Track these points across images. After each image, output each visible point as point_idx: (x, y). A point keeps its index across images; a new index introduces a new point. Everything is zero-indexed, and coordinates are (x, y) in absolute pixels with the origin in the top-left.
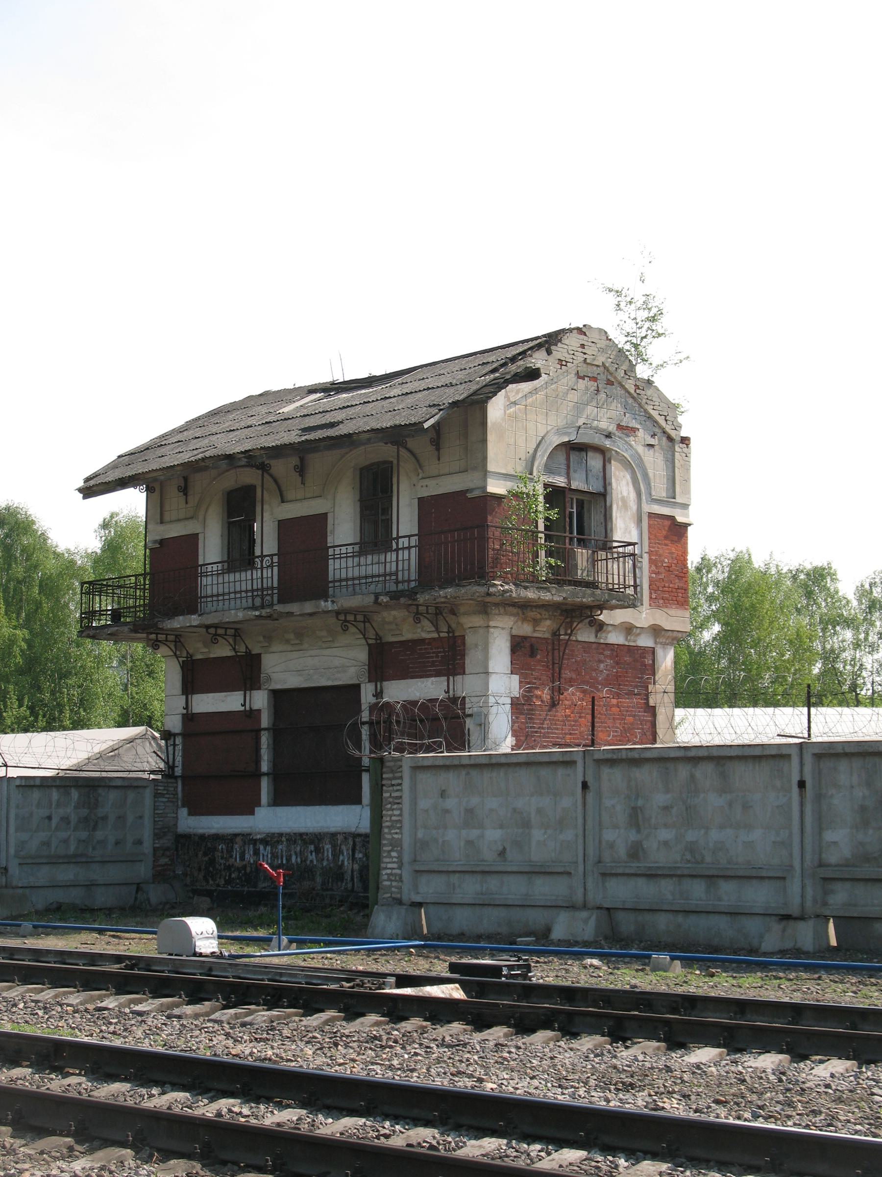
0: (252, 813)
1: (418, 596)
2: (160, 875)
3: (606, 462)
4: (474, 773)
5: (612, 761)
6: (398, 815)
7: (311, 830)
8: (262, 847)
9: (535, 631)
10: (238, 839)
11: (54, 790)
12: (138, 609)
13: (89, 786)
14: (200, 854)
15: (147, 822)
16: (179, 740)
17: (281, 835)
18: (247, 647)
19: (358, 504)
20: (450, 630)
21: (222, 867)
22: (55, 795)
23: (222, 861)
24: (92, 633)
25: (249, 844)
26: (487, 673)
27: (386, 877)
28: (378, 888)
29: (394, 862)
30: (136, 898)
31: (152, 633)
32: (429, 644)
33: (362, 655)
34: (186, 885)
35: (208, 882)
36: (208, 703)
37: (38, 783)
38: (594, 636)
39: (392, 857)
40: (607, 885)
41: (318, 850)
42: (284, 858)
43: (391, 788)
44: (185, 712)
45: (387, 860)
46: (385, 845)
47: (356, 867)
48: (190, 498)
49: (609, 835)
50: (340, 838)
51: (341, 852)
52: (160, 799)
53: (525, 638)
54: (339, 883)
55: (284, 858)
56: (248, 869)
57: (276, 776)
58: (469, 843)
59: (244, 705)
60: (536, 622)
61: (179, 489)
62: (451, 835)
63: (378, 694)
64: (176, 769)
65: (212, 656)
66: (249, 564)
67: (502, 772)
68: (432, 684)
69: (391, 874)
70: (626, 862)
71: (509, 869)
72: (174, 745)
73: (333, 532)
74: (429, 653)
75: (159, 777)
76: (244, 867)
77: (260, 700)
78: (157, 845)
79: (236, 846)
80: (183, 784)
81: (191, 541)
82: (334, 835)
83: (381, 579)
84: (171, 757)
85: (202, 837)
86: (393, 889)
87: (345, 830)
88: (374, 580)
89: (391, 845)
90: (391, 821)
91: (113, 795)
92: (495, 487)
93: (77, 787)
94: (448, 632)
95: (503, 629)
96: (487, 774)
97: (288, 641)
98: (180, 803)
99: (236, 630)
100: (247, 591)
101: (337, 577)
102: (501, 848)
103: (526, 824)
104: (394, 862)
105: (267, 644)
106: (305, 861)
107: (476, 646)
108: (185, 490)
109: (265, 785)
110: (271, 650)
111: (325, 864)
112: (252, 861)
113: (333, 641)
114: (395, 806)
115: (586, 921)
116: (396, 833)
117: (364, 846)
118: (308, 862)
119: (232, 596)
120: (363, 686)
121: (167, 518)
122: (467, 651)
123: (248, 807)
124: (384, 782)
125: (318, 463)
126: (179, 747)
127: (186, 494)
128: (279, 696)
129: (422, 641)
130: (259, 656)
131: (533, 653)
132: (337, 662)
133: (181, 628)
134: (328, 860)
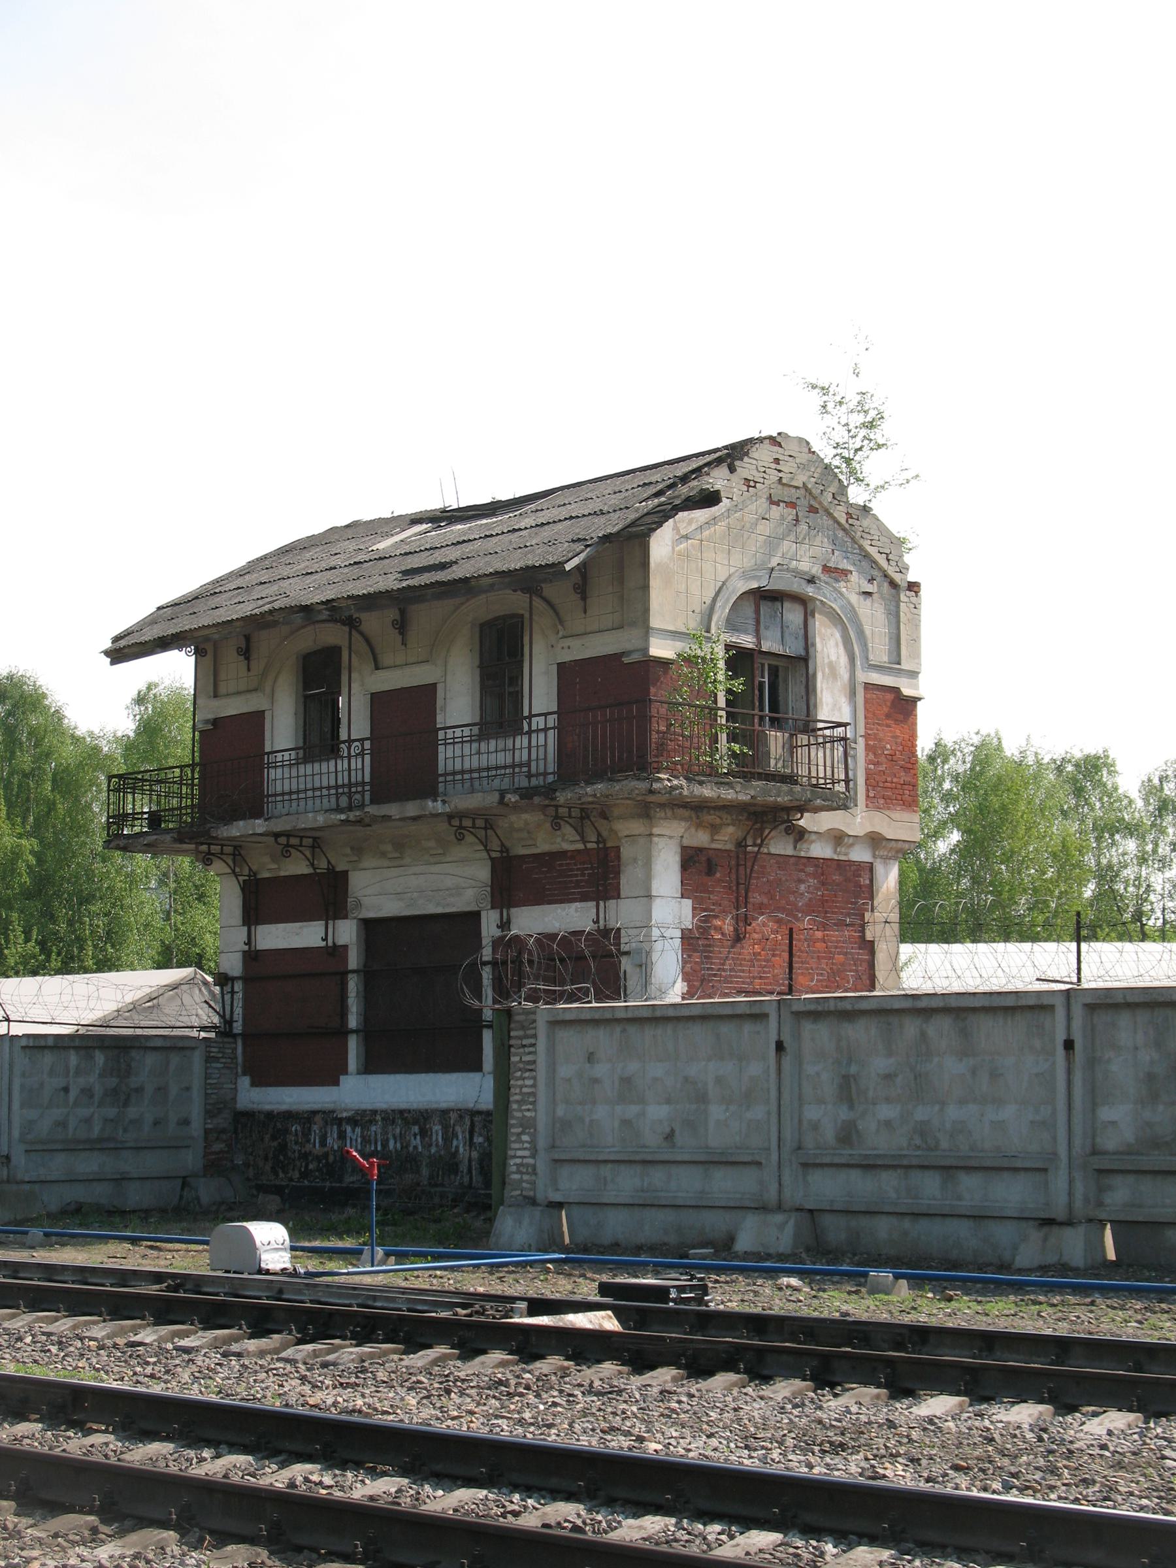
0: (336, 1083)
1: (558, 794)
2: (214, 1166)
3: (808, 615)
4: (632, 1029)
5: (816, 1014)
6: (531, 1086)
7: (415, 1106)
8: (349, 1129)
9: (713, 840)
10: (318, 1118)
11: (72, 1052)
12: (184, 811)
13: (118, 1048)
14: (267, 1137)
15: (197, 1095)
16: (238, 986)
17: (374, 1112)
18: (329, 862)
19: (478, 671)
20: (600, 839)
21: (297, 1154)
22: (73, 1059)
23: (297, 1148)
24: (122, 843)
25: (332, 1125)
26: (649, 897)
27: (514, 1168)
28: (504, 1183)
29: (525, 1149)
30: (181, 1197)
31: (202, 844)
32: (572, 858)
33: (483, 873)
34: (248, 1179)
35: (277, 1175)
36: (277, 936)
37: (50, 1042)
38: (792, 847)
39: (523, 1142)
40: (810, 1178)
41: (424, 1133)
42: (379, 1144)
43: (522, 1050)
44: (246, 948)
45: (516, 1146)
46: (513, 1126)
47: (475, 1155)
48: (253, 664)
49: (812, 1113)
50: (453, 1116)
51: (455, 1135)
52: (214, 1065)
53: (700, 850)
54: (452, 1177)
55: (379, 1144)
56: (331, 1158)
57: (368, 1034)
58: (626, 1123)
59: (325, 939)
60: (714, 829)
61: (239, 651)
62: (601, 1112)
63: (505, 925)
64: (235, 1025)
65: (283, 874)
66: (332, 751)
67: (669, 1028)
68: (576, 911)
69: (521, 1165)
70: (834, 1149)
71: (679, 1158)
72: (233, 992)
73: (444, 709)
74: (572, 870)
75: (213, 1035)
76: (326, 1155)
77: (347, 932)
78: (210, 1126)
79: (315, 1127)
80: (244, 1044)
81: (255, 721)
82: (445, 1113)
83: (508, 771)
84: (228, 1008)
85: (270, 1115)
86: (524, 1185)
87: (460, 1106)
88: (499, 772)
89: (521, 1125)
90: (521, 1093)
91: (150, 1059)
92: (660, 649)
93: (102, 1048)
94: (597, 843)
95: (671, 837)
96: (649, 1032)
97: (383, 855)
98: (240, 1070)
99: (315, 839)
100: (329, 788)
101: (450, 768)
102: (668, 1130)
103: (702, 1098)
104: (525, 1149)
105: (356, 858)
106: (407, 1147)
107: (635, 860)
108: (246, 653)
109: (353, 1045)
110: (362, 865)
111: (433, 1151)
112: (336, 1147)
113: (444, 854)
114: (527, 1074)
115: (781, 1227)
116: (529, 1110)
117: (485, 1126)
118: (411, 1149)
119: (310, 793)
120: (483, 914)
121: (222, 690)
122: (622, 868)
123: (331, 1076)
124: (512, 1042)
125: (424, 617)
126: (239, 996)
127: (248, 659)
128: (371, 928)
129: (563, 854)
130: (345, 874)
131: (710, 870)
132: (449, 882)
133: (241, 836)
134: (437, 1145)
